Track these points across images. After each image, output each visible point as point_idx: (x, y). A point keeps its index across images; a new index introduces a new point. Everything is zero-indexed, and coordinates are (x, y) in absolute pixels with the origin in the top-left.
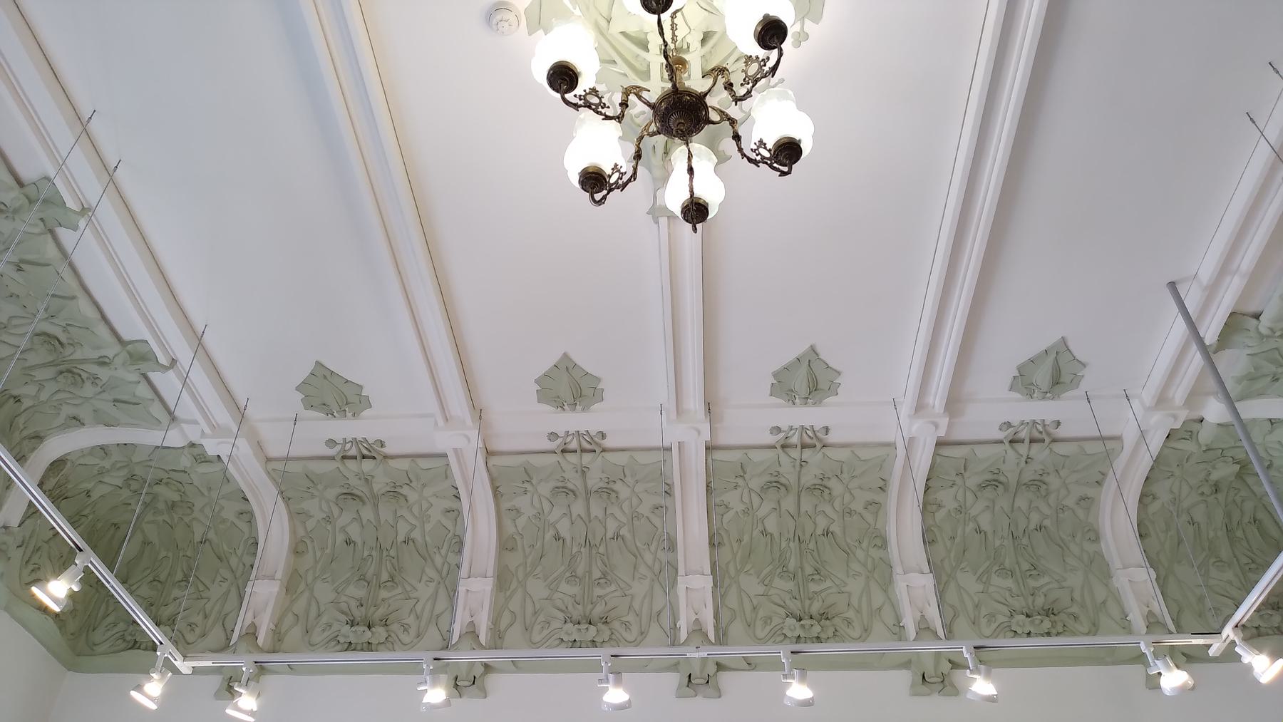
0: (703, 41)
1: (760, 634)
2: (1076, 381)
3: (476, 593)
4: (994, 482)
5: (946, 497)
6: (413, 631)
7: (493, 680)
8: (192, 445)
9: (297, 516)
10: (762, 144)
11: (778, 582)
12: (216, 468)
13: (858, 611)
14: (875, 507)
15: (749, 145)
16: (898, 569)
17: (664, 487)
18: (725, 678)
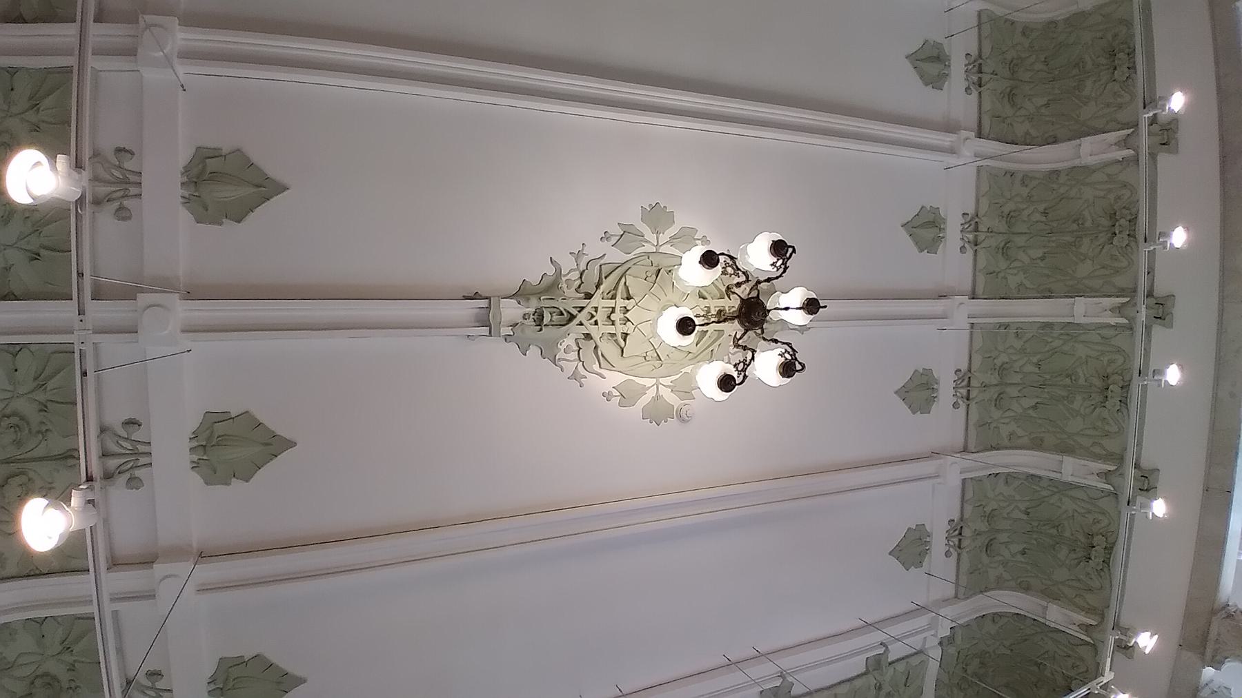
0: (704, 298)
1: (1125, 263)
2: (938, 46)
3: (1072, 469)
4: (1011, 96)
5: (1020, 129)
6: (1100, 517)
7: (1145, 463)
8: (940, 644)
9: (1000, 584)
10: (773, 264)
11: (1083, 249)
12: (959, 632)
13: (1110, 191)
14: (1026, 178)
15: (774, 272)
16: (1077, 162)
17: (1002, 330)
18: (1160, 290)
